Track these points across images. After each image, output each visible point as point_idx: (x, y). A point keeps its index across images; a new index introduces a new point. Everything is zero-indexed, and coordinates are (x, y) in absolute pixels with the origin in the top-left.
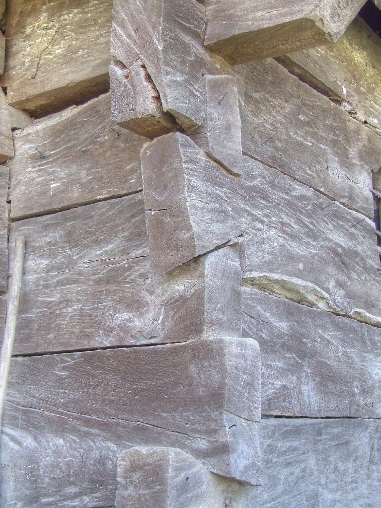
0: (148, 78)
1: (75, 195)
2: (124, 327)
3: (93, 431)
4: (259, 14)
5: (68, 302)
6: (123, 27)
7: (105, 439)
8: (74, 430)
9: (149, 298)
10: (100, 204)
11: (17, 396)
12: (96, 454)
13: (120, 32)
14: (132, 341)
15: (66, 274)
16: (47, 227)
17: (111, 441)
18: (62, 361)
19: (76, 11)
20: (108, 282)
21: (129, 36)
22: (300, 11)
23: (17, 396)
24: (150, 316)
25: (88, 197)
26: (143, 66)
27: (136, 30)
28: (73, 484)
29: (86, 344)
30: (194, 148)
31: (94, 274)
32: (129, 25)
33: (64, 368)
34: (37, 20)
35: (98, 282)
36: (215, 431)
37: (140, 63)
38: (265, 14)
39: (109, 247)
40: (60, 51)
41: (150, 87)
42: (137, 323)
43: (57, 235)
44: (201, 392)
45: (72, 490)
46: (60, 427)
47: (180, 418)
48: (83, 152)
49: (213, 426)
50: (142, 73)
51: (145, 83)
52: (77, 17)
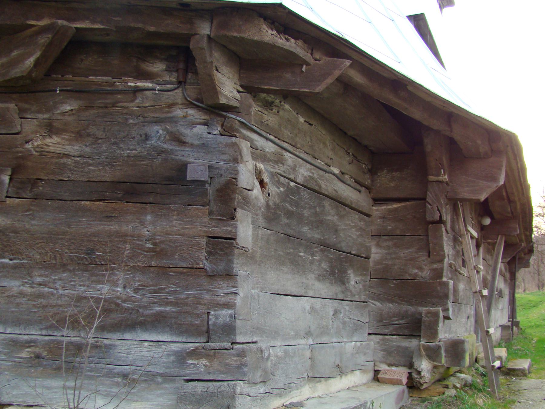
0: (438, 210)
1: (398, 232)
2: (416, 275)
3: (403, 303)
4: (465, 194)
5: (395, 265)
6: (431, 193)
7: (408, 305)
8: (396, 302)
9: (424, 267)
10: (406, 237)
11: (252, 219)
12: (404, 309)
13: (430, 195)
14: (418, 279)
15: (394, 256)
16: (386, 240)
17: (409, 306)
18: (392, 282)
19: (398, 173)
20: (410, 261)
21: (433, 197)
22: (477, 197)
23: (252, 219)
24: (425, 273)
25: (403, 234)
26: (437, 206)
27: (435, 196)
28: (396, 317)
29: (401, 278)
30: (492, 258)
31: (405, 258)
32: (433, 194)
33: (393, 284)
34: (383, 172)
35: (406, 260)
36: (445, 305)
37: (436, 205)
38: (468, 195)
39: (410, 250)
40: (393, 185)
41: (439, 213)
42: (420, 274)
43: (390, 243)
44: (441, 294)
45: (395, 319)
46: (391, 301)
47: (434, 300)
48: (401, 219)
49: (445, 303)
50: (437, 208)
51: (438, 211)
52: (399, 175)
